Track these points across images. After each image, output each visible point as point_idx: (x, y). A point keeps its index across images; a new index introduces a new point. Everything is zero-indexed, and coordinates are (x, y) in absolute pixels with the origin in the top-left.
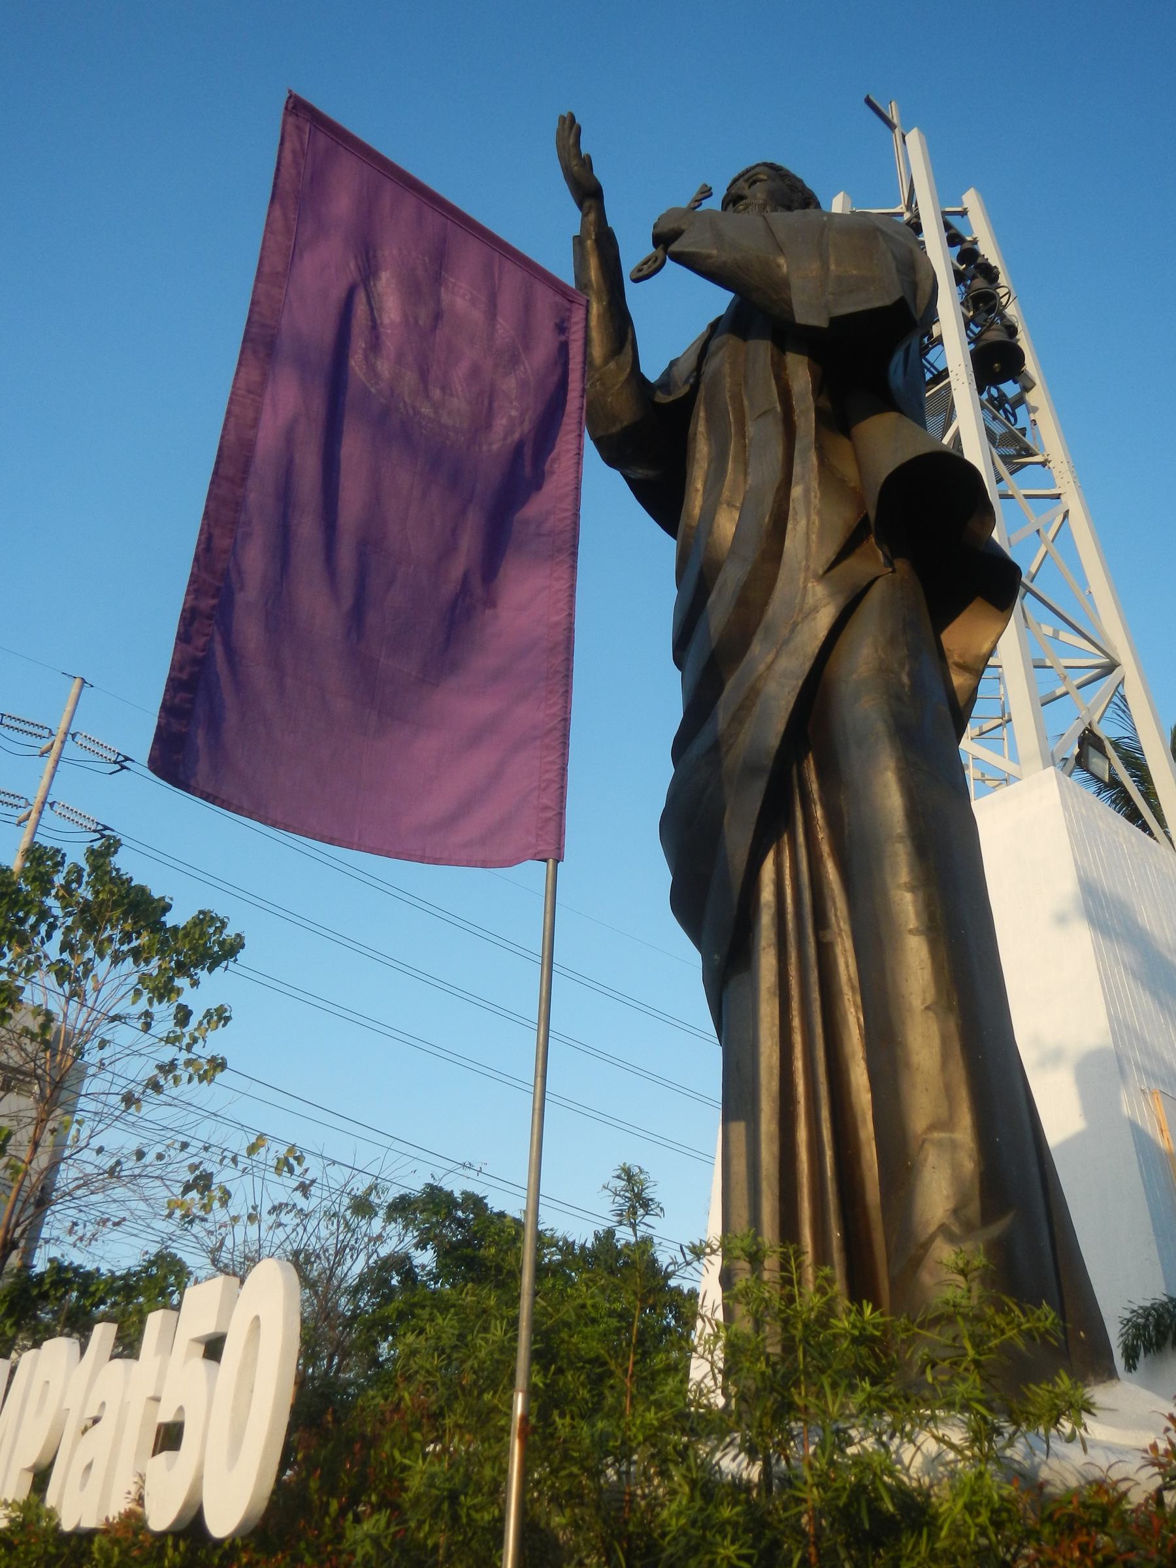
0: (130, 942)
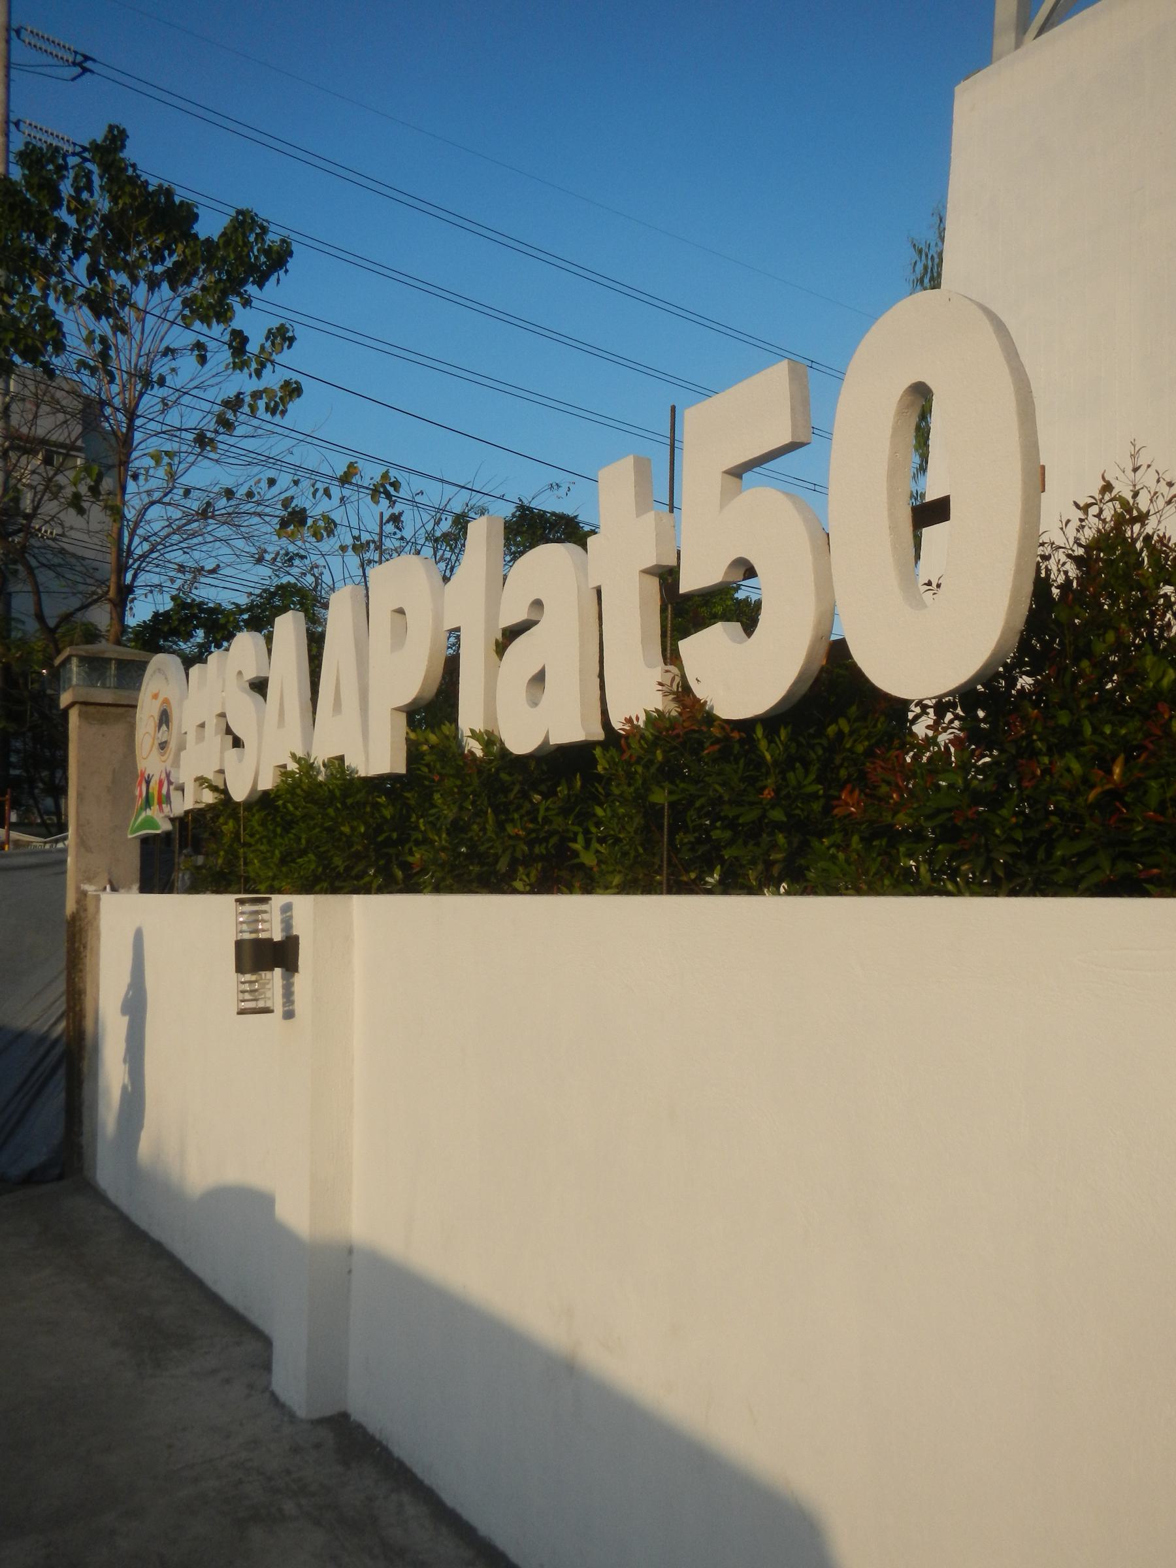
0: (163, 259)
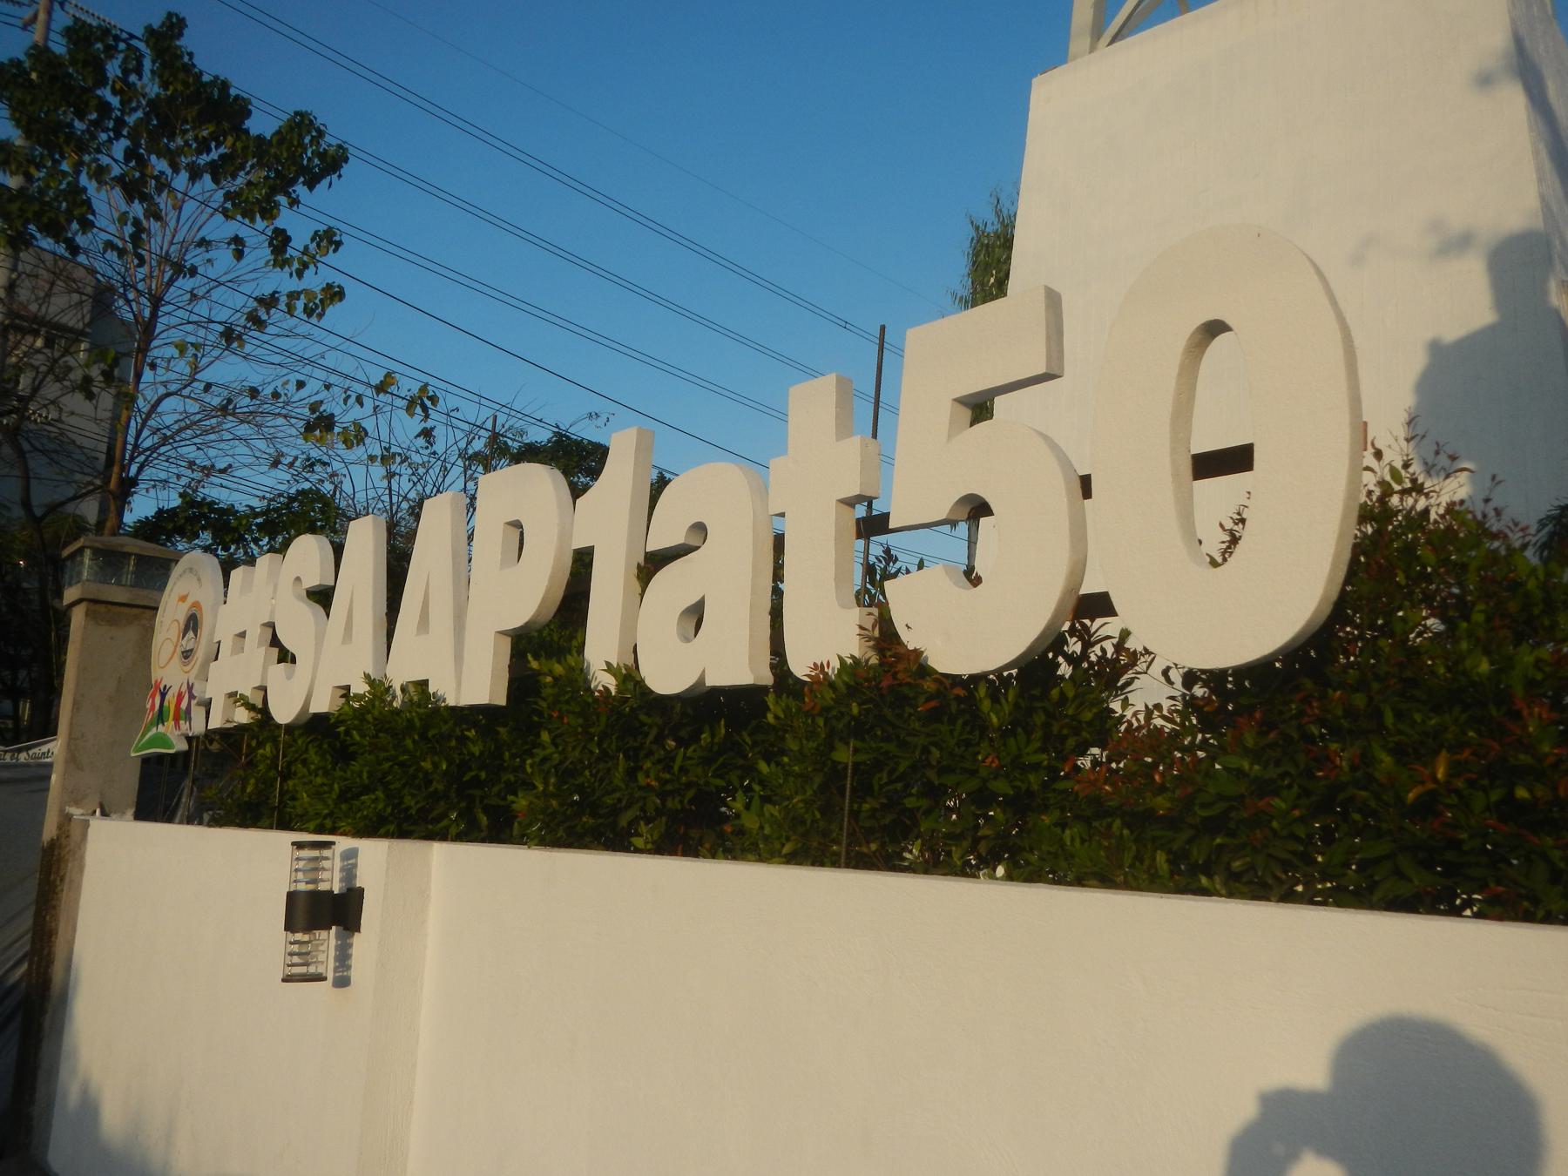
0: (209, 151)
